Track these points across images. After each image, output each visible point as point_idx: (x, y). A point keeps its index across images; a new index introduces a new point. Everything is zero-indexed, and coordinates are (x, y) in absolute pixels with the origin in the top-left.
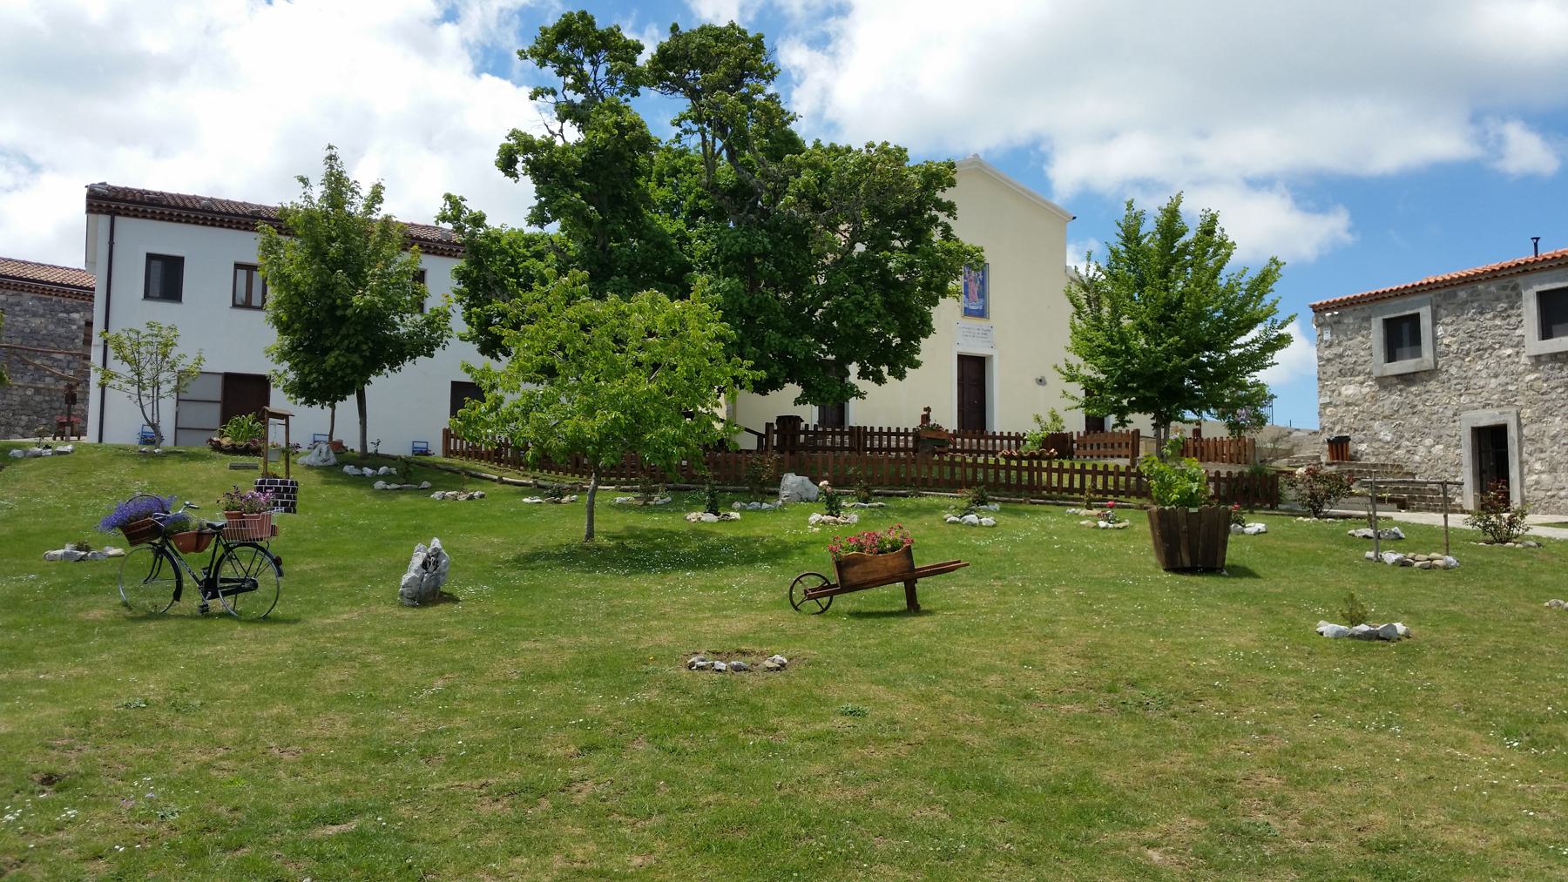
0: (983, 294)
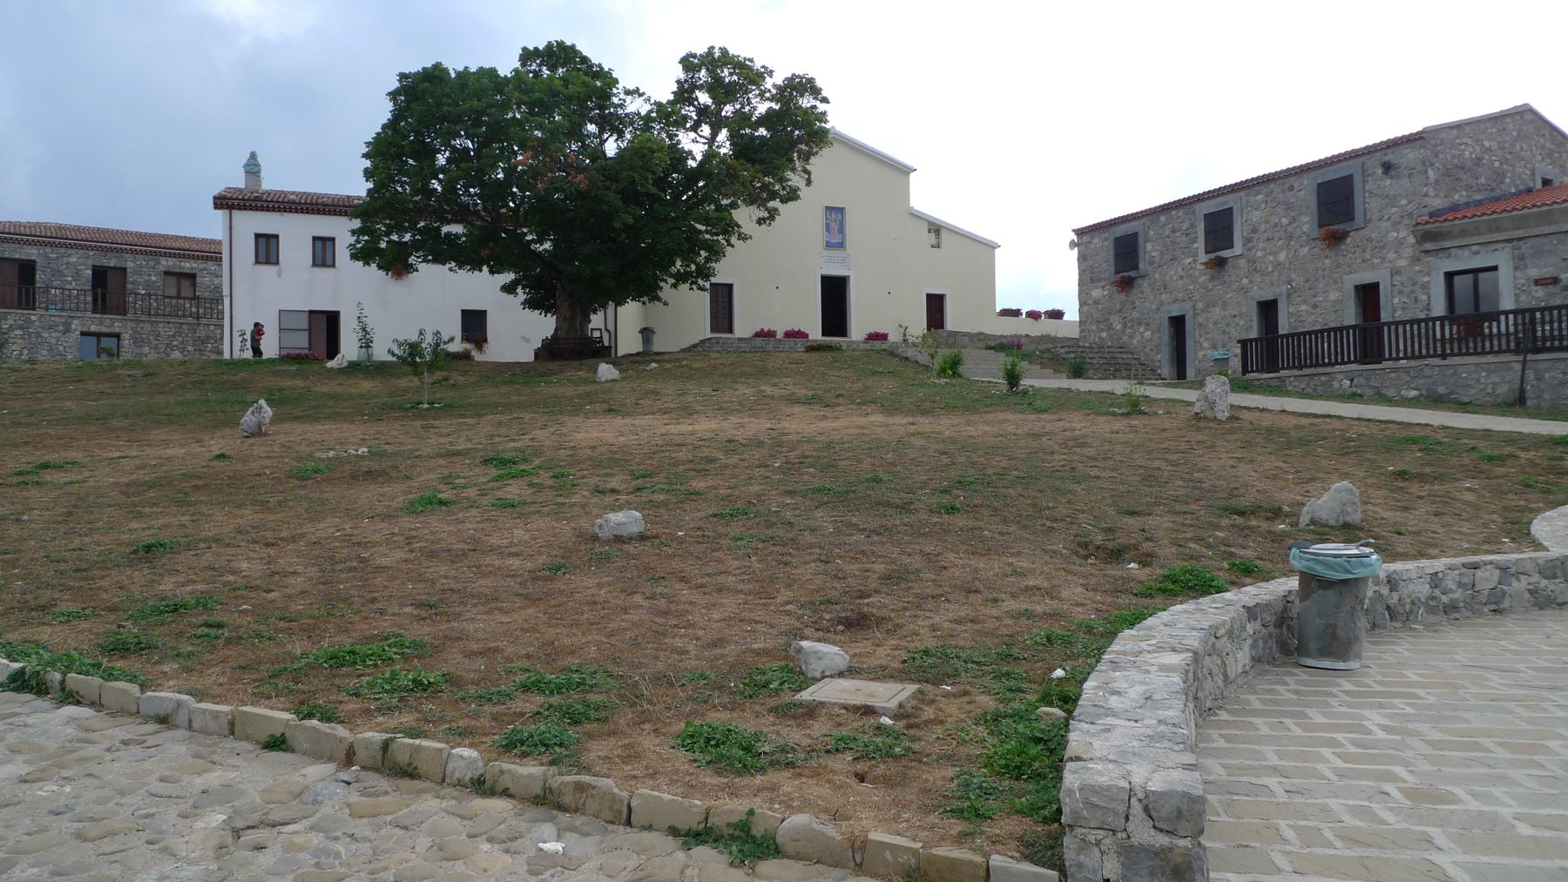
0: (841, 230)
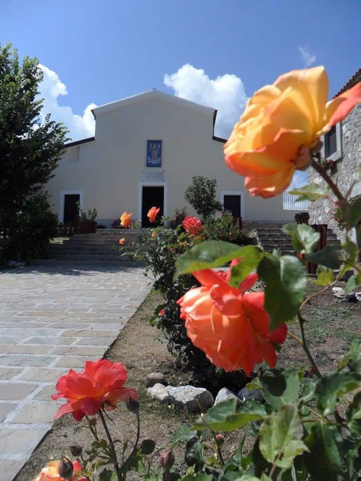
0: (159, 155)
